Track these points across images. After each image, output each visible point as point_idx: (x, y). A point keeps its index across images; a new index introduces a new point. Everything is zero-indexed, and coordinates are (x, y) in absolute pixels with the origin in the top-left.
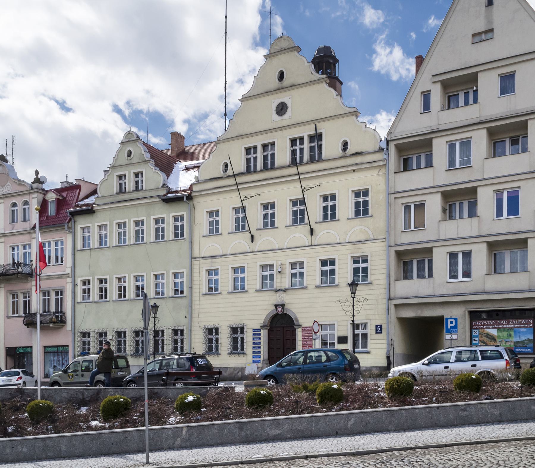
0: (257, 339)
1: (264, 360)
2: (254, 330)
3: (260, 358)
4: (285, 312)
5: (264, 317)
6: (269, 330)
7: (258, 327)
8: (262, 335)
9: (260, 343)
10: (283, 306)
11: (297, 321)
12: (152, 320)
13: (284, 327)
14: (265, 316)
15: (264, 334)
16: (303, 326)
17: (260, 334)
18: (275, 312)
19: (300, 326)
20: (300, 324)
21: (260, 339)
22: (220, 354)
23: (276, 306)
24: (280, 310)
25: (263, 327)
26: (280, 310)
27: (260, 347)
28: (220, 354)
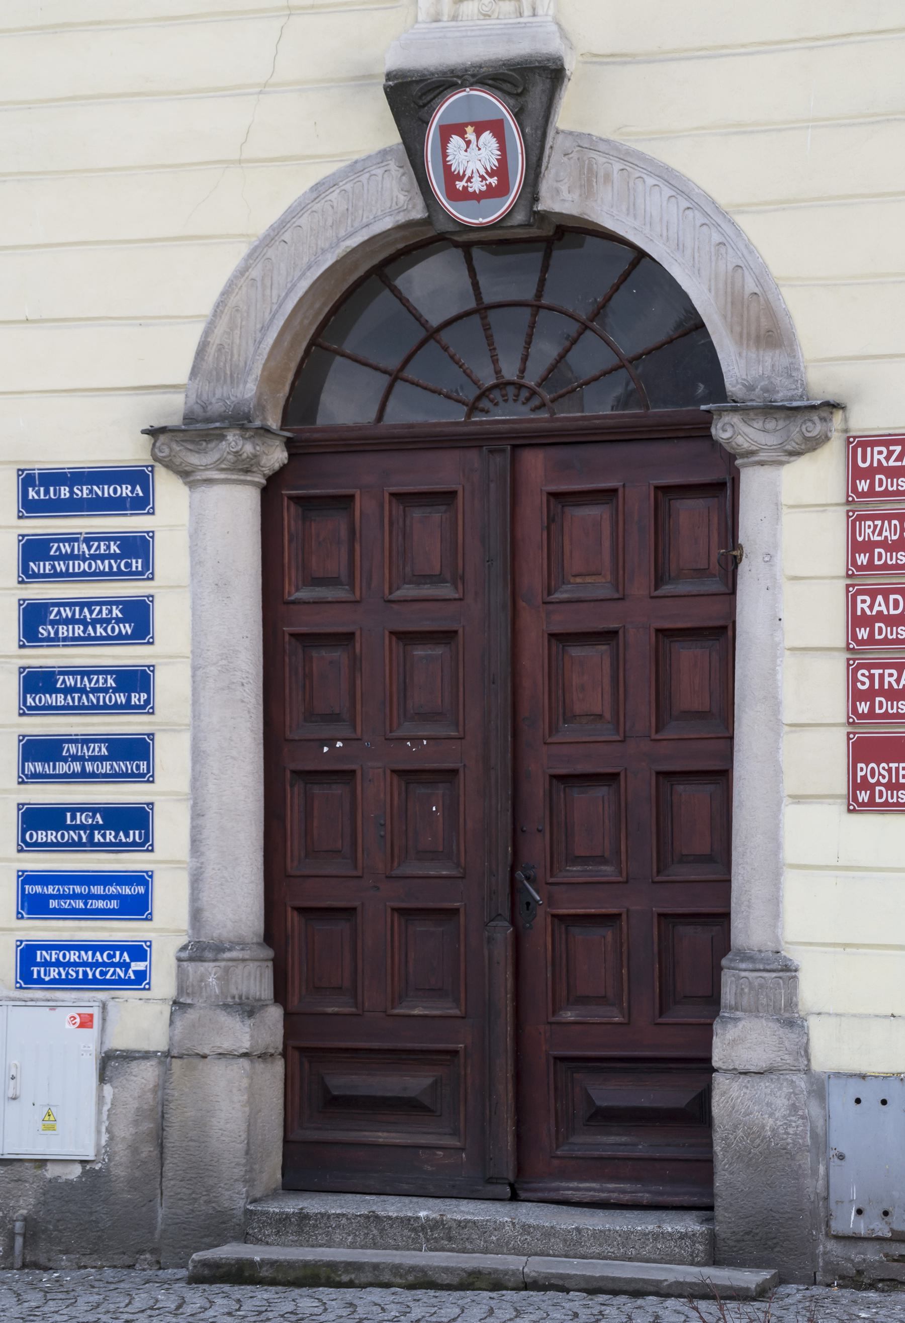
0: (87, 622)
1: (196, 951)
2: (44, 490)
3: (137, 907)
4: (560, 197)
5: (198, 283)
6: (271, 492)
8: (170, 556)
9: (136, 681)
10: (529, 84)
11: (771, 333)
12: (564, 936)
13: (520, 441)
14: (226, 262)
15: (204, 551)
16: (866, 419)
17: (138, 548)
18: (390, 204)
19: (805, 416)
20: (821, 381)
21: (138, 619)
22: (144, 432)
23: (413, 97)
24: (474, 158)
25: (188, 436)
26: (474, 158)
27: (134, 752)
28: (144, 432)
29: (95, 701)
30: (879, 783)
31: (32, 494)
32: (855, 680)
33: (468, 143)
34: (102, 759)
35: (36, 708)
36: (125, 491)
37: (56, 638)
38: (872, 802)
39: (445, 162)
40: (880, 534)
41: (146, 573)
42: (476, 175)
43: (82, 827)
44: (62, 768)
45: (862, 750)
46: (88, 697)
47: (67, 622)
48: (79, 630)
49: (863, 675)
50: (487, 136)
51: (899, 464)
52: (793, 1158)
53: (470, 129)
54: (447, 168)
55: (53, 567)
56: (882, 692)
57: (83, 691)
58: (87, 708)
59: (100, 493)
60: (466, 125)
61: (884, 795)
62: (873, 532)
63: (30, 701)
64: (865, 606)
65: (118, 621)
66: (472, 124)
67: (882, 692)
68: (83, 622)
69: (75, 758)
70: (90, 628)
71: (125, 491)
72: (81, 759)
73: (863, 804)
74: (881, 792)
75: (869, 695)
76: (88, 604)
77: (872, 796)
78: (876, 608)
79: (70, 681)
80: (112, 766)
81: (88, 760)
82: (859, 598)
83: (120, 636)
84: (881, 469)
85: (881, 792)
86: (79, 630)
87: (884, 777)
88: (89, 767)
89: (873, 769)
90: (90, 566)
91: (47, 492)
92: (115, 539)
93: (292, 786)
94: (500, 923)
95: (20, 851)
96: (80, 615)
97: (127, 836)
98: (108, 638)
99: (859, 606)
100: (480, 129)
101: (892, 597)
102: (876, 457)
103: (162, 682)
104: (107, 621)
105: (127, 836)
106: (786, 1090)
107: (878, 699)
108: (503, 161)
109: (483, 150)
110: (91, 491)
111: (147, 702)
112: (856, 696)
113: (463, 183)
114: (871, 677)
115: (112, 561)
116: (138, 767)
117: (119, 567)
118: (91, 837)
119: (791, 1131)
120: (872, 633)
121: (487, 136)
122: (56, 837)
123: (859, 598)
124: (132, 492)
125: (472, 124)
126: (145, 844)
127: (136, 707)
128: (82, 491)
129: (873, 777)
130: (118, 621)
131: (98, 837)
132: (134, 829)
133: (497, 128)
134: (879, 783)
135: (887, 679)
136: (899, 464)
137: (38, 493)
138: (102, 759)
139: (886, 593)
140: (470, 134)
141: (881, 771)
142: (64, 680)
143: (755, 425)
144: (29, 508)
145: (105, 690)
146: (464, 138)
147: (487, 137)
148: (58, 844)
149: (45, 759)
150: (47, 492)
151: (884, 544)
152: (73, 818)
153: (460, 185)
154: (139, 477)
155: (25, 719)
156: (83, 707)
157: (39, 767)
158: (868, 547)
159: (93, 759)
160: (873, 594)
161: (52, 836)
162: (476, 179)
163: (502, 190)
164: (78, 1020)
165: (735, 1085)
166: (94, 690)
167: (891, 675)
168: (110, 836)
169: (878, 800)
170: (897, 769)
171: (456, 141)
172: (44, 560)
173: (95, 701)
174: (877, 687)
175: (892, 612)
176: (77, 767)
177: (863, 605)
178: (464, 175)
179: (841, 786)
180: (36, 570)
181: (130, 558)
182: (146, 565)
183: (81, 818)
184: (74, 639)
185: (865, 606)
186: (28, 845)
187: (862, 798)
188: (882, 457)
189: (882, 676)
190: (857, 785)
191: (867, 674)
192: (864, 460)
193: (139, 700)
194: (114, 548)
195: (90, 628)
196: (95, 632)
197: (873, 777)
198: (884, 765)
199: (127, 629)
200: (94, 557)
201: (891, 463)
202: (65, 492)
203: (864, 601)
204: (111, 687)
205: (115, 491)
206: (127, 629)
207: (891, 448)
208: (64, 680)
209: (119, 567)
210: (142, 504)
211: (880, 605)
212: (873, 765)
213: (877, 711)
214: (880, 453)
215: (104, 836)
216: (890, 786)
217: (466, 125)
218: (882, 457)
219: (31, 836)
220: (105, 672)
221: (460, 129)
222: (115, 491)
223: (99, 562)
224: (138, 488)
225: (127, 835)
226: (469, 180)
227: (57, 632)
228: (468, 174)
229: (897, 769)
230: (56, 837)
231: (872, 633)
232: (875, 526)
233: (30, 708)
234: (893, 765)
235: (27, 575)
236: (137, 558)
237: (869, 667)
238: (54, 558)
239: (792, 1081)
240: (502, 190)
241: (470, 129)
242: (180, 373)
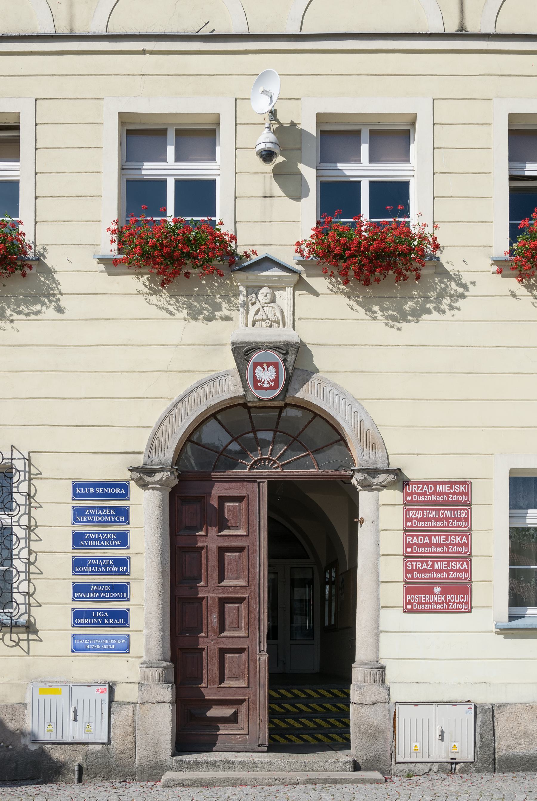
0: (102, 541)
2: (81, 489)
7: (115, 470)
15: (146, 510)
24: (266, 375)
25: (144, 473)
26: (266, 375)
27: (121, 590)
30: (415, 602)
31: (78, 491)
32: (406, 566)
33: (264, 369)
34: (107, 592)
36: (118, 491)
37: (88, 546)
39: (254, 375)
40: (415, 515)
43: (99, 617)
44: (91, 595)
45: (408, 591)
46: (101, 569)
47: (92, 539)
48: (98, 543)
52: (384, 733)
53: (265, 365)
54: (255, 378)
55: (87, 519)
57: (99, 566)
60: (264, 363)
61: (416, 606)
63: (76, 569)
65: (114, 540)
66: (266, 363)
67: (416, 570)
68: (100, 540)
69: (96, 591)
71: (118, 491)
72: (99, 592)
73: (409, 609)
74: (415, 605)
75: (411, 571)
76: (102, 533)
77: (412, 607)
79: (94, 562)
82: (408, 537)
83: (115, 545)
85: (415, 605)
86: (98, 543)
92: (113, 509)
95: (73, 626)
97: (118, 621)
100: (269, 365)
101: (419, 537)
102: (413, 488)
104: (110, 540)
105: (118, 621)
106: (382, 709)
108: (277, 377)
110: (103, 490)
111: (127, 570)
112: (407, 571)
113: (261, 384)
114: (412, 565)
116: (123, 595)
117: (115, 519)
118: (103, 621)
119: (384, 724)
120: (412, 550)
123: (408, 537)
124: (120, 491)
125: (266, 363)
127: (122, 572)
130: (114, 540)
131: (106, 621)
133: (276, 365)
134: (415, 602)
137: (80, 490)
138: (107, 592)
139: (417, 536)
140: (265, 366)
141: (415, 598)
144: (76, 496)
145: (109, 566)
147: (272, 368)
149: (83, 592)
151: (416, 519)
152: (96, 614)
153: (259, 384)
156: (100, 572)
158: (410, 520)
159: (103, 592)
160: (413, 536)
161: (86, 621)
163: (276, 387)
164: (100, 690)
165: (364, 709)
167: (419, 564)
168: (111, 621)
170: (421, 597)
171: (259, 368)
172: (83, 516)
175: (419, 542)
176: (97, 595)
179: (401, 603)
182: (126, 519)
183: (98, 614)
184: (95, 546)
185: (410, 540)
186: (76, 624)
187: (409, 608)
188: (415, 489)
189: (416, 565)
190: (407, 603)
194: (112, 512)
196: (104, 543)
199: (118, 543)
200: (104, 515)
201: (419, 491)
202: (92, 490)
203: (409, 539)
206: (118, 543)
209: (115, 519)
210: (125, 496)
211: (415, 540)
212: (412, 596)
214: (415, 487)
215: (109, 621)
216: (419, 603)
217: (264, 363)
218: (415, 489)
220: (109, 559)
221: (261, 365)
226: (263, 382)
227: (88, 543)
228: (263, 380)
229: (421, 597)
231: (412, 550)
233: (77, 572)
234: (420, 596)
236: (122, 516)
237: (411, 561)
240: (276, 387)
241: (265, 365)
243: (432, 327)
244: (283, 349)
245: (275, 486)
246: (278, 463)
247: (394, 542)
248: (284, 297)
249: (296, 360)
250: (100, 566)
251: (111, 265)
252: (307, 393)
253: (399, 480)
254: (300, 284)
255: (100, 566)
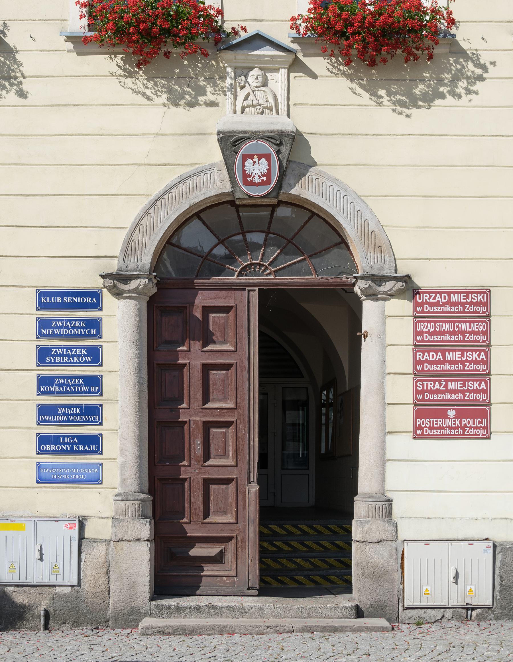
2: (47, 299)
5: (129, 213)
8: (107, 329)
15: (120, 322)
25: (118, 280)
26: (257, 169)
27: (93, 413)
29: (74, 390)
30: (426, 427)
31: (43, 300)
32: (416, 386)
33: (255, 162)
34: (77, 414)
35: (45, 392)
36: (88, 300)
37: (55, 362)
38: (423, 434)
39: (243, 169)
40: (427, 328)
41: (99, 335)
42: (257, 176)
45: (418, 414)
47: (60, 355)
48: (66, 359)
49: (420, 384)
50: (263, 160)
51: (434, 301)
53: (256, 157)
54: (244, 172)
55: (53, 332)
56: (427, 391)
57: (68, 385)
58: (70, 393)
59: (76, 301)
60: (254, 155)
62: (424, 328)
63: (42, 389)
64: (420, 357)
65: (85, 356)
66: (257, 155)
67: (427, 391)
68: (68, 356)
69: (64, 414)
70: (71, 358)
71: (88, 300)
72: (67, 414)
73: (419, 435)
74: (426, 430)
75: (422, 392)
77: (423, 432)
78: (425, 358)
80: (82, 418)
81: (70, 415)
82: (418, 353)
84: (427, 303)
85: (426, 430)
86: (66, 359)
87: (428, 424)
88: (71, 418)
89: (423, 421)
90: (71, 332)
91: (50, 299)
92: (83, 321)
93: (157, 428)
94: (254, 485)
96: (66, 353)
98: (80, 363)
99: (418, 356)
100: (260, 157)
102: (425, 298)
103: (106, 382)
104: (80, 356)
107: (425, 394)
109: (261, 165)
110: (72, 300)
113: (251, 178)
114: (423, 385)
115: (82, 330)
116: (94, 418)
117: (85, 332)
118: (72, 448)
119: (390, 564)
121: (263, 160)
122: (55, 448)
123: (418, 353)
124: (91, 301)
125: (257, 155)
126: (99, 451)
127: (93, 392)
128: (67, 299)
129: (423, 424)
130: (85, 356)
131: (75, 448)
132: (93, 445)
133: (268, 157)
135: (429, 386)
136: (434, 301)
138: (77, 414)
140: (256, 158)
142: (59, 380)
143: (377, 283)
145: (79, 385)
146: (253, 160)
148: (56, 451)
149: (49, 415)
150: (50, 299)
151: (428, 332)
152: (64, 440)
153: (249, 179)
154: (96, 295)
155: (39, 397)
156: (68, 392)
157: (47, 418)
158: (421, 333)
159: (72, 414)
160: (424, 352)
161: (53, 448)
162: (257, 177)
163: (268, 182)
164: (69, 526)
165: (368, 547)
166: (73, 385)
168: (81, 448)
169: (425, 434)
170: (433, 421)
171: (249, 161)
172: (49, 329)
173: (74, 390)
174: (425, 389)
175: (431, 359)
177: (419, 356)
178: (251, 175)
180: (45, 333)
181: (91, 329)
182: (98, 332)
183: (67, 440)
185: (420, 357)
186: (41, 451)
187: (419, 433)
188: (427, 298)
189: (427, 385)
190: (417, 428)
191: (421, 383)
192: (420, 299)
193: (95, 389)
194: (82, 324)
195: (71, 358)
196: (73, 360)
197: (423, 424)
198: (428, 420)
199: (89, 359)
200: (73, 328)
201: (431, 301)
202: (59, 300)
203: (420, 355)
204: (82, 384)
205: (83, 300)
207: (431, 295)
208: (59, 380)
209: (85, 332)
210: (97, 306)
213: (425, 398)
214: (426, 296)
217: (254, 155)
218: (427, 298)
219: (43, 448)
221: (251, 157)
222: (83, 300)
223: (75, 330)
224: (94, 299)
225: (89, 448)
226: (254, 177)
228: (253, 175)
229: (433, 421)
230: (55, 448)
232: (425, 325)
233: (42, 392)
234: (432, 420)
235: (40, 335)
236: (94, 329)
237: (422, 381)
238: (54, 328)
239: (391, 545)
240: (268, 182)
241: (256, 157)
242: (117, 250)
243: (445, 114)
244: (277, 139)
245: (267, 295)
246: (271, 269)
247: (402, 359)
248: (278, 80)
249: (291, 151)
250: (69, 387)
251: (80, 43)
252: (305, 190)
253: (409, 288)
254: (295, 65)
255: (69, 387)
